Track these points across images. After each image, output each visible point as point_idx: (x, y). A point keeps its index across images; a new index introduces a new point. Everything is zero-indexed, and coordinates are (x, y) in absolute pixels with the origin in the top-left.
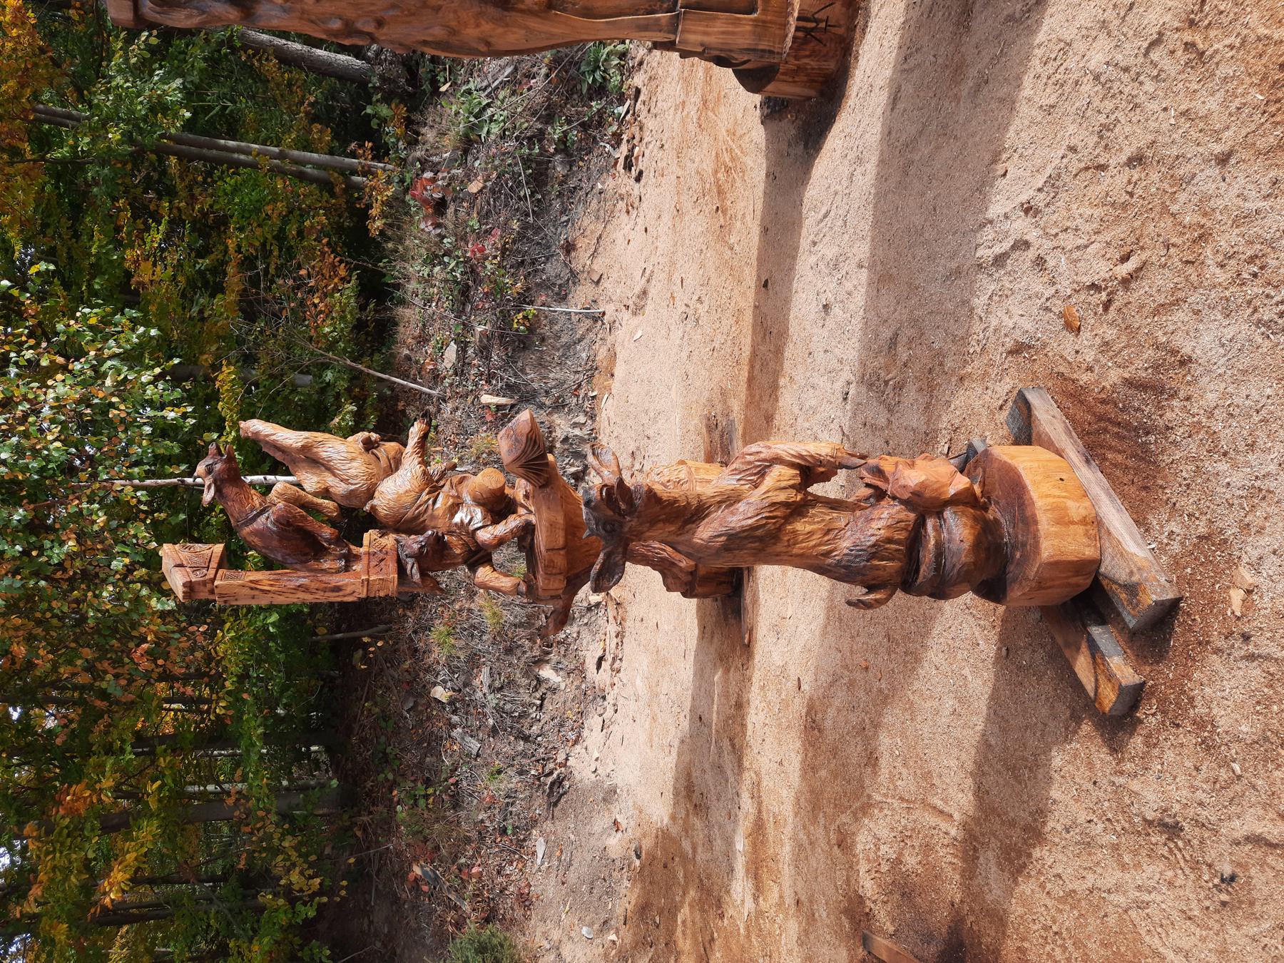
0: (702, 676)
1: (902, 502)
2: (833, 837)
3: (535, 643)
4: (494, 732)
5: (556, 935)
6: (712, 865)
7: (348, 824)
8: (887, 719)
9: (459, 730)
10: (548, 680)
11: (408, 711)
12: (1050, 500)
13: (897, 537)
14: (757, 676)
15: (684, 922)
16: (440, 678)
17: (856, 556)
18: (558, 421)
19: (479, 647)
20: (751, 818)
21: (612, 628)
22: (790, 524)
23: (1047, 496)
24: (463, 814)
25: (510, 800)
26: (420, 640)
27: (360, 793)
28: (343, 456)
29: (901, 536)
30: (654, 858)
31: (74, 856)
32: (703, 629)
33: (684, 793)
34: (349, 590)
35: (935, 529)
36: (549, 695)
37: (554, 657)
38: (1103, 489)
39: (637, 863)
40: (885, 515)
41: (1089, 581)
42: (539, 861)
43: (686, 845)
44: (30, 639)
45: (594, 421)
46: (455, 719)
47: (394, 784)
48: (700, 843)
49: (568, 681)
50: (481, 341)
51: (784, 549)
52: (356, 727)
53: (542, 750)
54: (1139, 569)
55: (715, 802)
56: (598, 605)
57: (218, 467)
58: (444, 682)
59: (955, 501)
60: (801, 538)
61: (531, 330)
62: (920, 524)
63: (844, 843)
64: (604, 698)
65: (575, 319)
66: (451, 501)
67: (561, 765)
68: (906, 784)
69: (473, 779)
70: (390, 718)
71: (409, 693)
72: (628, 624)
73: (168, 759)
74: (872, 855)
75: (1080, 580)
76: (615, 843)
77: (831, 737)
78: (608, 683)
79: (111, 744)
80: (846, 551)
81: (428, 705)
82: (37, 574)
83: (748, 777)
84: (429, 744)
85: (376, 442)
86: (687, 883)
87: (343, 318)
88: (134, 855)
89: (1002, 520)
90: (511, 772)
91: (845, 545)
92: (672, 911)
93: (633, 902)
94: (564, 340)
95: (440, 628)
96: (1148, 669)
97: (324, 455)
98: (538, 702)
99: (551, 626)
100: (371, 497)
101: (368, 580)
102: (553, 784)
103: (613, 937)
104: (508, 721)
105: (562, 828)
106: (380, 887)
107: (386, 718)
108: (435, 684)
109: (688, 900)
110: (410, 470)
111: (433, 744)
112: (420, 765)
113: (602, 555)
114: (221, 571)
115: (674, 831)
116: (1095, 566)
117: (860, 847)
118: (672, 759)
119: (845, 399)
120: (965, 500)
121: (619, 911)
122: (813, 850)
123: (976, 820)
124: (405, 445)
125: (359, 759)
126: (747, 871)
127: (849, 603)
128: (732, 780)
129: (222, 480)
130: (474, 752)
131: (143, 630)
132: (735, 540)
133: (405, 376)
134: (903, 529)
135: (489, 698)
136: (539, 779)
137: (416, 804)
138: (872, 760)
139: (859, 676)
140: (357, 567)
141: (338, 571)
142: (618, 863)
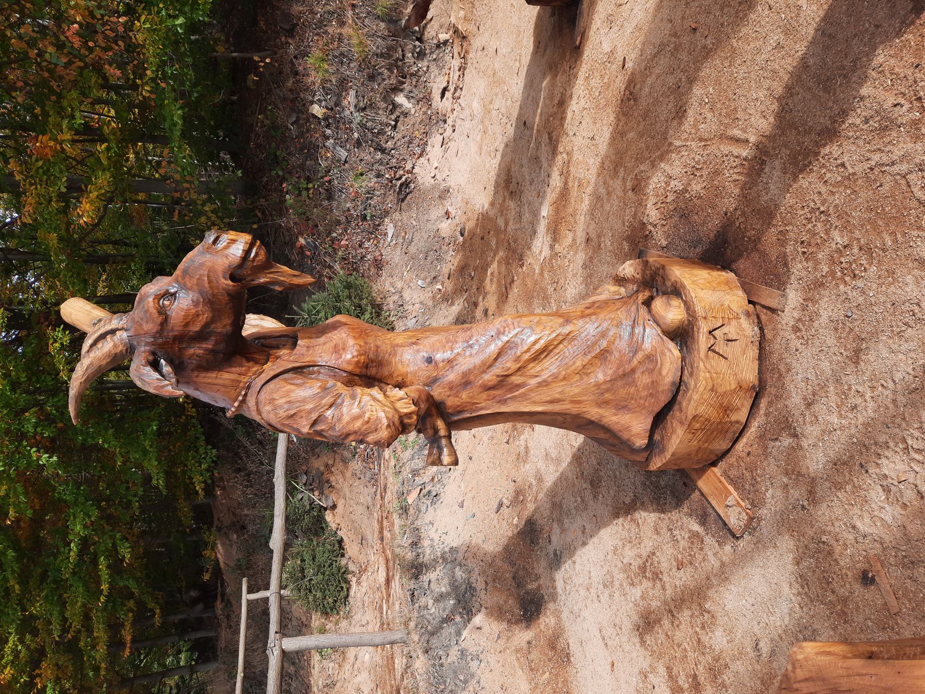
0: (531, 87)
3: (393, 73)
4: (358, 144)
5: (399, 285)
6: (519, 232)
7: (251, 207)
9: (332, 141)
10: (402, 105)
15: (492, 274)
16: (316, 98)
20: (558, 190)
21: (456, 63)
24: (335, 204)
31: (51, 189)
32: (538, 44)
33: (503, 185)
36: (401, 119)
39: (461, 239)
42: (389, 239)
43: (501, 222)
46: (328, 132)
47: (284, 179)
49: (418, 108)
52: (253, 136)
55: (528, 187)
56: (446, 42)
58: (320, 101)
64: (445, 121)
67: (410, 172)
69: (342, 179)
70: (278, 129)
71: (292, 110)
76: (445, 227)
77: (643, 103)
78: (449, 109)
83: (560, 159)
84: (309, 151)
86: (497, 248)
88: (96, 194)
92: (485, 267)
93: (456, 264)
95: (316, 53)
98: (393, 123)
102: (402, 185)
103: (440, 287)
105: (409, 217)
106: (277, 251)
107: (275, 127)
108: (312, 103)
109: (497, 258)
111: (311, 151)
115: (492, 213)
121: (446, 271)
122: (608, 200)
123: (771, 138)
126: (548, 230)
128: (545, 165)
130: (343, 159)
136: (391, 182)
137: (300, 194)
142: (447, 240)
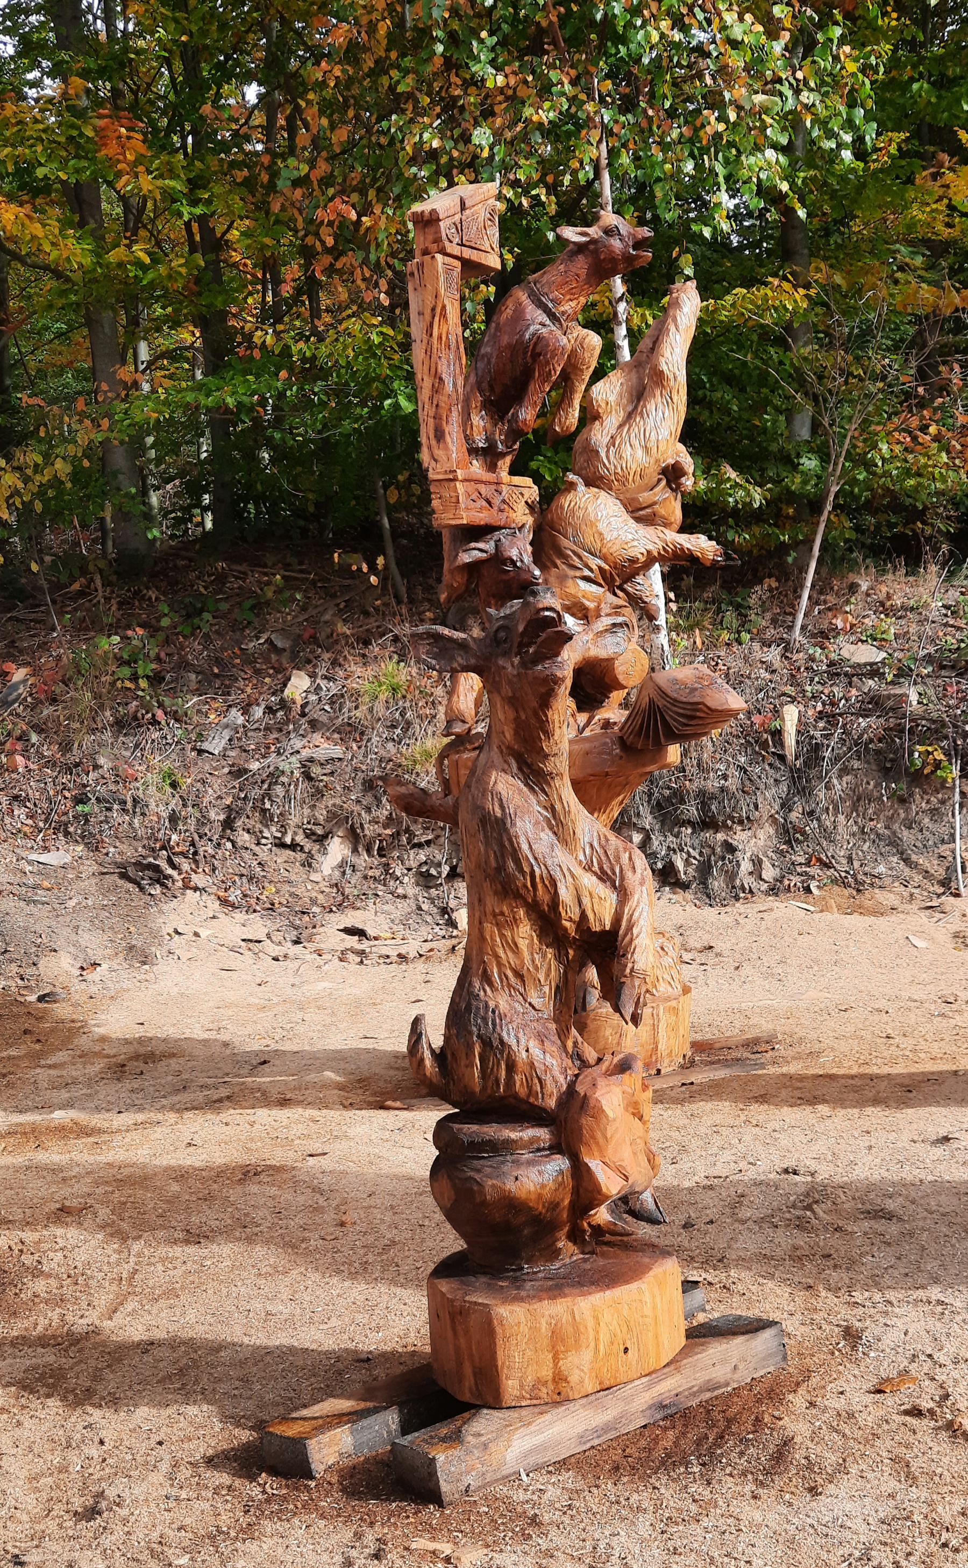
1: (571, 1086)
2: (73, 1203)
3: (385, 827)
4: (238, 772)
6: (29, 1089)
8: (259, 1250)
9: (241, 720)
11: (269, 641)
12: (590, 1323)
13: (517, 1078)
14: (335, 1115)
16: (323, 683)
17: (485, 1019)
18: (761, 834)
19: (375, 739)
21: (412, 947)
22: (527, 914)
23: (596, 1319)
24: (108, 736)
25: (129, 805)
26: (383, 647)
27: (141, 578)
28: (648, 435)
29: (520, 1088)
30: (39, 1019)
31: (39, 148)
33: (142, 1050)
34: (439, 453)
35: (533, 1140)
36: (300, 856)
37: (363, 860)
38: (617, 1420)
39: (33, 998)
40: (549, 1059)
41: (467, 1397)
42: (34, 857)
43: (61, 1056)
44: (352, 53)
45: (767, 893)
46: (258, 712)
47: (152, 629)
48: (64, 1073)
49: (323, 886)
50: (889, 697)
51: (489, 908)
52: (244, 567)
53: (211, 851)
54: (485, 1446)
55: (129, 1086)
56: (452, 924)
57: (616, 244)
59: (580, 1171)
60: (508, 934)
61: (918, 778)
62: (536, 1116)
63: (64, 1213)
64: (297, 942)
65: (944, 849)
66: (591, 605)
68: (157, 1276)
70: (258, 615)
71: (297, 640)
72: (420, 966)
73: (183, 270)
74: (45, 1246)
75: (469, 1381)
76: (60, 967)
78: (322, 946)
79: (204, 187)
80: (492, 1004)
81: (278, 670)
82: (453, 40)
84: (217, 676)
85: (679, 485)
87: (907, 473)
89: (558, 1265)
90: (175, 803)
91: (501, 1001)
94: (905, 834)
95: (403, 673)
96: (334, 1480)
97: (651, 406)
98: (288, 840)
99: (403, 790)
100: (590, 483)
101: (455, 479)
102: (157, 869)
104: (256, 793)
108: (313, 676)
110: (637, 540)
111: (218, 680)
112: (184, 665)
113: (463, 635)
114: (457, 264)
115: (83, 1042)
116: (491, 1401)
117: (59, 1231)
118: (199, 1033)
119: (786, 1171)
120: (584, 1191)
124: (682, 530)
125: (192, 575)
127: (417, 1022)
129: (596, 252)
130: (205, 746)
131: (377, 211)
132: (497, 830)
133: (821, 587)
134: (530, 1088)
135: (293, 759)
136: (163, 848)
137: (122, 663)
138: (194, 1237)
139: (330, 1216)
140: (477, 467)
141: (468, 438)
142: (31, 970)
